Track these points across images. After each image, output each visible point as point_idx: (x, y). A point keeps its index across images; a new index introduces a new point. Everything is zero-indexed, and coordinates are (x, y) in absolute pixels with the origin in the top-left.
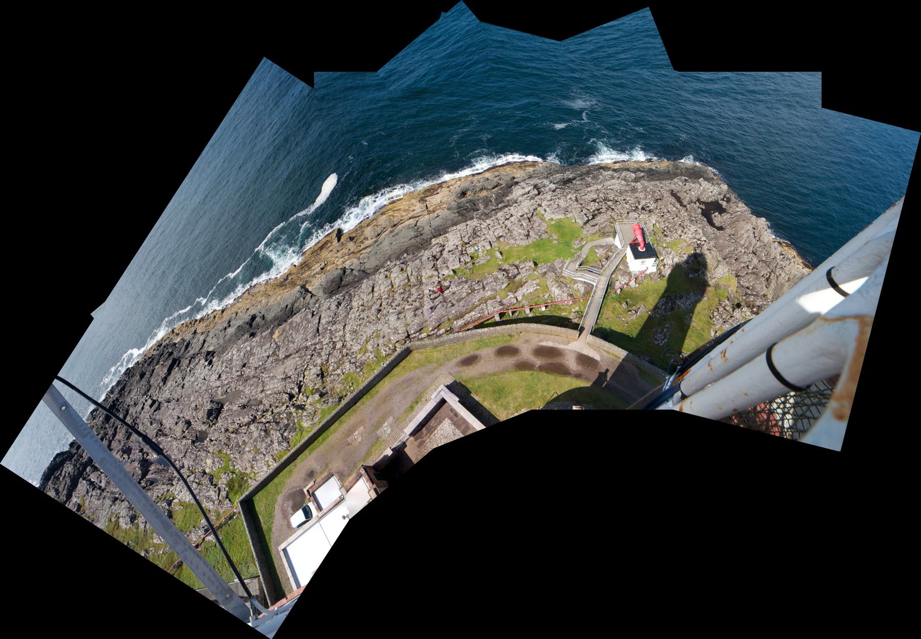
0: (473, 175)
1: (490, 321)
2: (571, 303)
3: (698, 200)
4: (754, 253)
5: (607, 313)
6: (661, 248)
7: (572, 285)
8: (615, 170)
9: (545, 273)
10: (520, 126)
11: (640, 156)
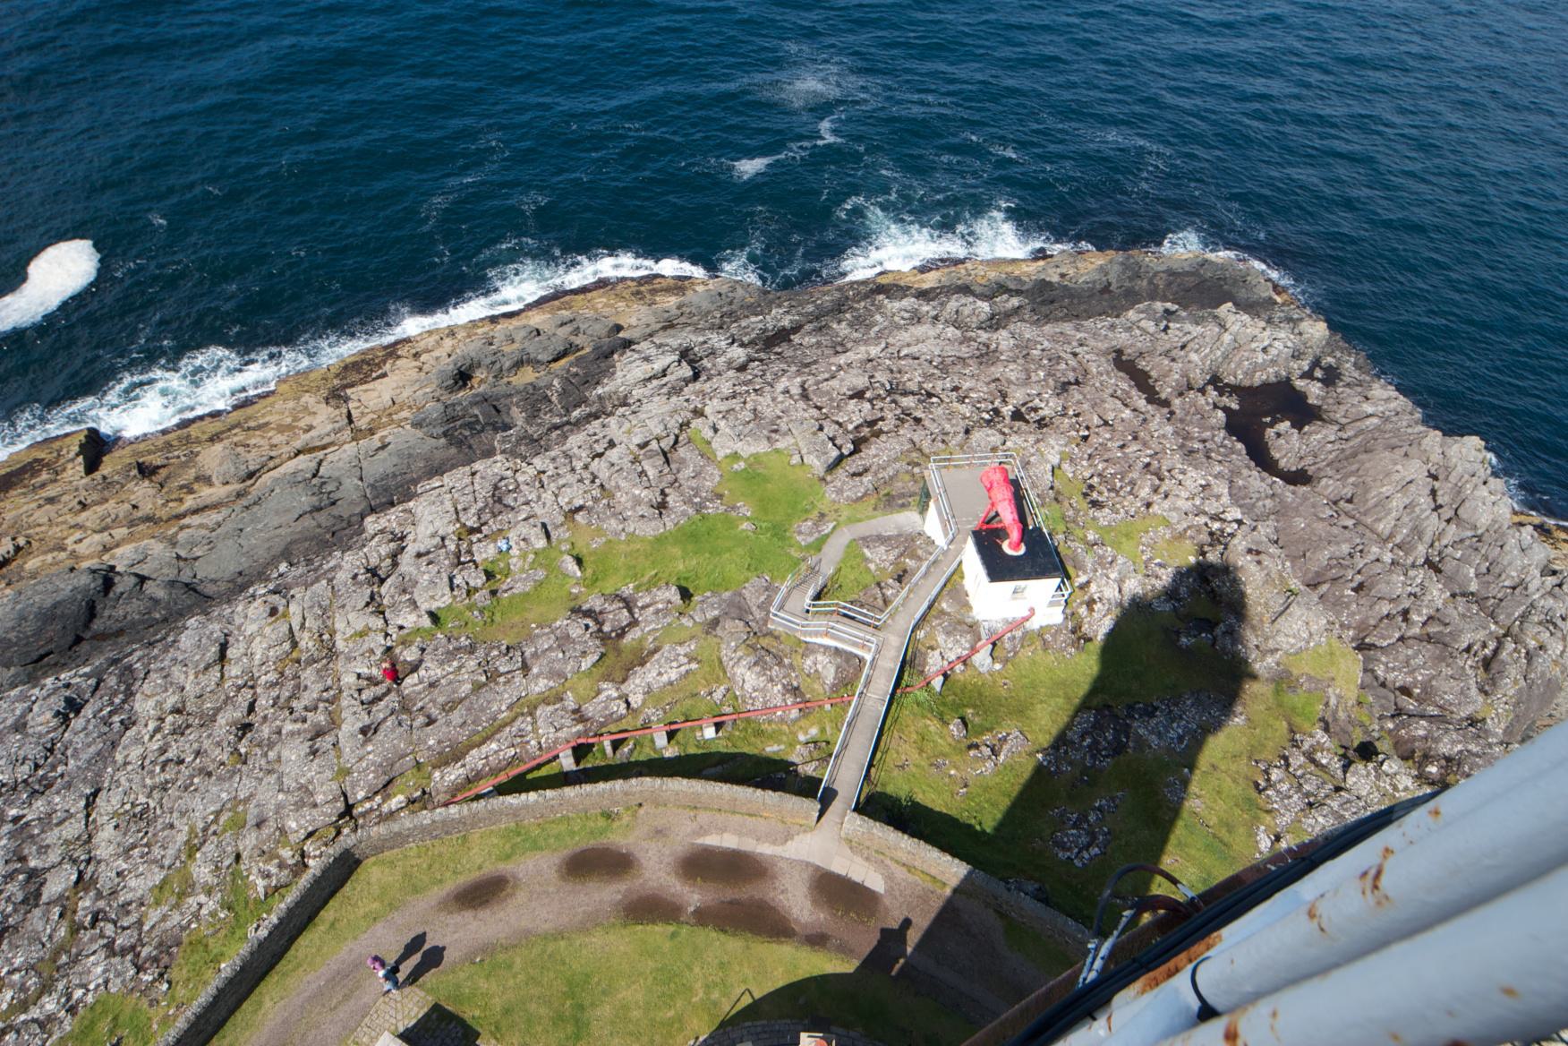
0: (493, 319)
1: (544, 772)
2: (794, 713)
3: (1215, 380)
4: (1429, 563)
5: (902, 749)
6: (1079, 547)
7: (797, 660)
8: (923, 295)
9: (715, 622)
10: (635, 168)
11: (1001, 243)
